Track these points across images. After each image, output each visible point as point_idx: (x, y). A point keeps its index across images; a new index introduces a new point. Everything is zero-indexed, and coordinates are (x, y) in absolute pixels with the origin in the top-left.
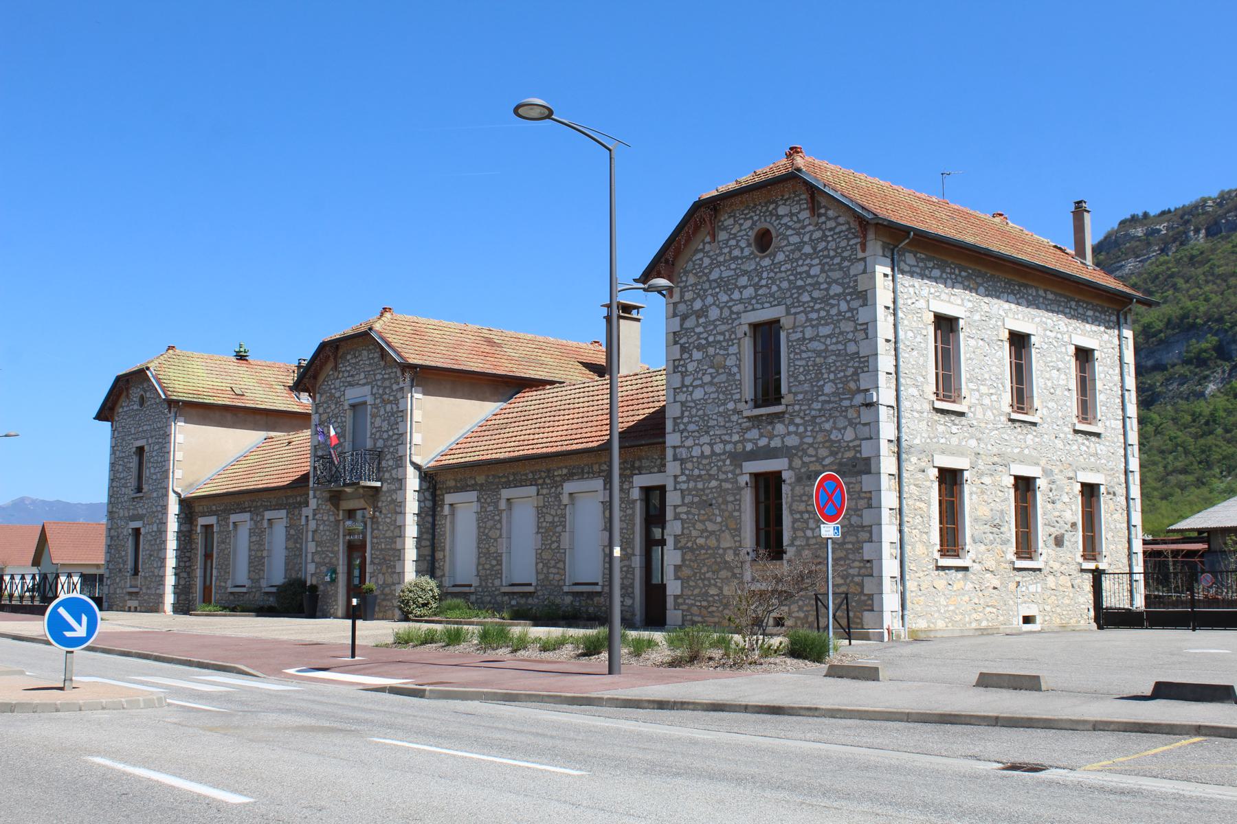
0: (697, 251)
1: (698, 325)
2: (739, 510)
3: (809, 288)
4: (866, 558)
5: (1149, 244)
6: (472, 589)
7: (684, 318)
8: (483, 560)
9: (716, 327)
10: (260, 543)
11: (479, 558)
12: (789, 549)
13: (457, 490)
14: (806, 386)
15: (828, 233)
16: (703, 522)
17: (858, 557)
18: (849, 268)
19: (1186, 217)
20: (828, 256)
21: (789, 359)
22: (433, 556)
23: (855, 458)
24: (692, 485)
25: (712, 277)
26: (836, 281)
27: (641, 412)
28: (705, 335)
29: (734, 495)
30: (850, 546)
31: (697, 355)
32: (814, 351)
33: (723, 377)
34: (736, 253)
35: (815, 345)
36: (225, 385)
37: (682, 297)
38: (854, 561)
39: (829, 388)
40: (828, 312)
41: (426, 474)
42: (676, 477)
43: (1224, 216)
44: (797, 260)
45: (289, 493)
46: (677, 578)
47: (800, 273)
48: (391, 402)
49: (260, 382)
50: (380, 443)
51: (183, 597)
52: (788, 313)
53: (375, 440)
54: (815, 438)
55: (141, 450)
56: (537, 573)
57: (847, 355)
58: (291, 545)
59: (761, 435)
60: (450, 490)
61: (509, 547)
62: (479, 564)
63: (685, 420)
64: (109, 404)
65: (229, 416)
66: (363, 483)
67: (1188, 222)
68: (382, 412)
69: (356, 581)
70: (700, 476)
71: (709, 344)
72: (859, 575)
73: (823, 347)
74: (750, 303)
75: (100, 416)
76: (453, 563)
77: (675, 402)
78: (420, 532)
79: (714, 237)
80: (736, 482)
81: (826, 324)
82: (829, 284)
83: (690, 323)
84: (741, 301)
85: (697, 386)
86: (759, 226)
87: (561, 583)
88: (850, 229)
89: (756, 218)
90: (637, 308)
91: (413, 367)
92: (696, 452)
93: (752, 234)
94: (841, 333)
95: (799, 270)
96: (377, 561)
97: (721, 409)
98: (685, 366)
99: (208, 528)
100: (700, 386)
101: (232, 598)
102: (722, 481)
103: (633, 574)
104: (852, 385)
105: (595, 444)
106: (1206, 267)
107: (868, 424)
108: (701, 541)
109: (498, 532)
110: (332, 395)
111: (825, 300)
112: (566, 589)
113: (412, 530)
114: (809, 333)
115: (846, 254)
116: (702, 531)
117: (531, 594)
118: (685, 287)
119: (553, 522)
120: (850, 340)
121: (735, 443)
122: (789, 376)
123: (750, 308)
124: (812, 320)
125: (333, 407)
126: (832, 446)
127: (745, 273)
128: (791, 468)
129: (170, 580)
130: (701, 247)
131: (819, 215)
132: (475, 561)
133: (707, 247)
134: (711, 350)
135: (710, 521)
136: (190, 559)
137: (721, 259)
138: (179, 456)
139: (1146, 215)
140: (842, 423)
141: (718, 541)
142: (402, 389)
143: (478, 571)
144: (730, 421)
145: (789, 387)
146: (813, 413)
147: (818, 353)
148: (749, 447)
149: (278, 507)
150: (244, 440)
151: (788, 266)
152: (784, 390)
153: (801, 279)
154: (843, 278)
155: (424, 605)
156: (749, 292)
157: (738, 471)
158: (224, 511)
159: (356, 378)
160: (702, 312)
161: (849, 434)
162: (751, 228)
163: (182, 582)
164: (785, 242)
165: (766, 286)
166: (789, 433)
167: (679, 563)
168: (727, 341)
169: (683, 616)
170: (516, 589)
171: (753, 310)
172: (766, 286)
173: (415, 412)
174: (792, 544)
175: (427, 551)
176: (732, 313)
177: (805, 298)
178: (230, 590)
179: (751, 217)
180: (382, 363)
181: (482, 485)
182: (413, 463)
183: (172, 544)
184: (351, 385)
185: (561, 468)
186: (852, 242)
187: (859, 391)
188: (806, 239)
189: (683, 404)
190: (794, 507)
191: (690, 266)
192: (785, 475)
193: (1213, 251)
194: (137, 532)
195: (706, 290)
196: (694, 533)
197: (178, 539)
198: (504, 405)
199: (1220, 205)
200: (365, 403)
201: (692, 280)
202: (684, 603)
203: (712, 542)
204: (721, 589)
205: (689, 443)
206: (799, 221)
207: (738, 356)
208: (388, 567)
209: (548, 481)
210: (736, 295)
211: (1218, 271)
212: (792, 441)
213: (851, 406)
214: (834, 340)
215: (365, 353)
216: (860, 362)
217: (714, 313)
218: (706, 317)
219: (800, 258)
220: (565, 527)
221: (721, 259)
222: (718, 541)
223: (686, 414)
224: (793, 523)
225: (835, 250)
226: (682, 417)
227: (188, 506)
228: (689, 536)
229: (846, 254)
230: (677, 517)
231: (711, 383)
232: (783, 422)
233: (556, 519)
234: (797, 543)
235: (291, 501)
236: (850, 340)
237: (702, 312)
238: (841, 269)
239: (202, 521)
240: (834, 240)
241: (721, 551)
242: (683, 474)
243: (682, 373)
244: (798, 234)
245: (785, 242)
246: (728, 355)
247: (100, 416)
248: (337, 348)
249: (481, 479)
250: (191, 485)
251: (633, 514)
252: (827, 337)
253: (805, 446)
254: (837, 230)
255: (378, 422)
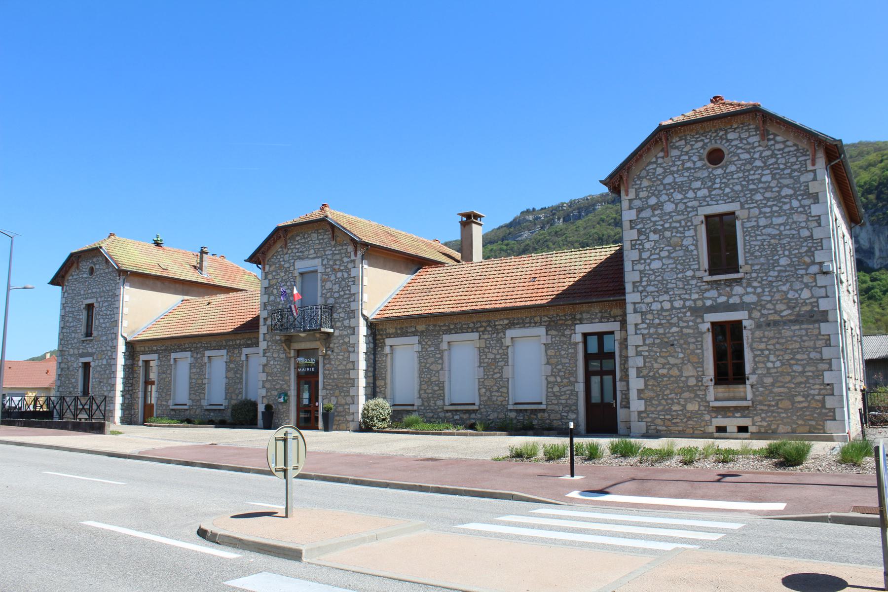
0: (650, 163)
1: (654, 216)
2: (702, 348)
3: (761, 191)
4: (826, 382)
5: (535, 224)
6: (415, 408)
7: (640, 210)
8: (425, 387)
9: (671, 217)
10: (201, 374)
11: (421, 385)
12: (750, 376)
13: (396, 335)
14: (762, 260)
15: (776, 152)
16: (665, 357)
17: (818, 381)
18: (799, 177)
19: (553, 212)
20: (778, 168)
21: (745, 240)
22: (374, 384)
23: (812, 310)
24: (652, 330)
25: (666, 181)
26: (787, 186)
27: (571, 280)
28: (661, 223)
29: (696, 338)
30: (810, 374)
31: (653, 237)
32: (769, 235)
33: (681, 253)
34: (689, 164)
35: (769, 231)
36: (154, 262)
37: (637, 195)
38: (814, 385)
39: (784, 261)
40: (781, 207)
41: (371, 323)
42: (636, 325)
43: (572, 212)
44: (748, 171)
45: (233, 337)
46: (640, 398)
47: (752, 180)
48: (342, 271)
49: (174, 261)
50: (331, 301)
51: (127, 412)
52: (742, 207)
53: (326, 299)
54: (772, 297)
55: (90, 307)
56: (480, 396)
57: (800, 237)
58: (231, 375)
59: (720, 295)
60: (389, 336)
61: (450, 377)
62: (420, 389)
63: (644, 284)
64: (62, 273)
65: (159, 284)
66: (323, 330)
67: (554, 214)
68: (333, 278)
69: (306, 402)
70: (660, 324)
71: (666, 229)
72: (819, 394)
73: (778, 232)
74: (705, 200)
75: (55, 281)
76: (393, 389)
77: (633, 270)
78: (367, 366)
79: (667, 154)
80: (698, 328)
81: (780, 216)
82: (781, 188)
83: (646, 214)
84: (695, 199)
85: (654, 259)
86: (710, 147)
87: (504, 403)
88: (797, 150)
89: (706, 141)
90: (480, 217)
91: (365, 245)
92: (656, 306)
93: (705, 153)
94: (795, 222)
95: (751, 177)
96: (329, 387)
97: (680, 276)
98: (642, 244)
99: (147, 363)
100: (658, 259)
101: (206, 413)
102: (682, 328)
103: (577, 396)
104: (807, 260)
105: (544, 302)
106: (563, 238)
107: (825, 287)
108: (664, 371)
109: (440, 367)
110: (281, 266)
111: (778, 198)
112: (510, 407)
113: (362, 365)
114: (763, 221)
115: (795, 167)
116: (664, 365)
117: (474, 411)
118: (639, 188)
119: (495, 359)
120: (803, 228)
121: (695, 301)
122: (745, 252)
123: (705, 203)
124: (765, 213)
125: (282, 274)
126: (789, 302)
127: (698, 179)
128: (750, 318)
129: (119, 400)
130: (654, 160)
131: (769, 140)
132: (417, 387)
133: (660, 161)
134: (667, 234)
135: (673, 356)
136: (132, 384)
137: (675, 169)
138: (126, 310)
139: (534, 209)
140: (798, 286)
141: (680, 370)
142: (354, 261)
143: (420, 395)
144: (688, 284)
145: (746, 260)
146: (770, 279)
147: (773, 237)
148: (709, 303)
149: (220, 347)
150: (169, 301)
151: (741, 175)
152: (741, 261)
153: (754, 184)
154: (794, 184)
155: (384, 420)
156: (705, 192)
157: (699, 320)
158: (165, 350)
159: (307, 253)
160: (659, 206)
161: (806, 294)
162: (702, 147)
163: (127, 401)
164: (736, 158)
165: (720, 188)
166: (747, 293)
167: (642, 387)
168: (684, 227)
169: (647, 426)
170: (459, 408)
171: (708, 205)
172: (720, 188)
173: (364, 278)
174: (753, 373)
175: (371, 380)
176: (687, 207)
177: (758, 197)
178: (171, 407)
179: (702, 140)
180: (333, 243)
181: (422, 332)
182: (363, 316)
183: (120, 374)
184: (300, 258)
185: (502, 320)
186: (800, 159)
187: (813, 263)
188: (757, 156)
189: (641, 272)
190: (755, 345)
191: (644, 173)
192: (745, 323)
193: (566, 229)
194: (87, 366)
195: (660, 191)
196: (656, 365)
197: (124, 370)
198: (413, 277)
199: (570, 206)
200: (316, 271)
201: (645, 183)
202: (648, 417)
203: (675, 372)
204: (684, 406)
205: (649, 300)
206: (748, 143)
207: (695, 238)
208: (340, 392)
209: (489, 329)
210: (691, 194)
211: (570, 239)
212: (750, 299)
213: (807, 274)
214: (788, 227)
215: (315, 235)
216: (813, 243)
217: (669, 207)
218: (662, 210)
219: (752, 169)
220: (507, 362)
221: (675, 169)
222: (680, 370)
223: (645, 279)
224: (755, 356)
225: (784, 164)
226: (641, 281)
227: (131, 346)
228: (651, 368)
229: (795, 167)
230: (638, 354)
231: (668, 257)
232: (741, 285)
233: (498, 357)
234: (759, 372)
235: (231, 343)
236: (803, 228)
237: (659, 206)
238: (791, 177)
239: (143, 357)
240: (783, 157)
241: (683, 379)
242: (643, 322)
243: (639, 250)
244: (749, 153)
245: (736, 158)
246: (685, 237)
247: (55, 281)
248: (286, 231)
249: (421, 328)
250: (133, 332)
251: (576, 353)
252: (780, 225)
253: (763, 303)
254: (786, 150)
255: (328, 285)
